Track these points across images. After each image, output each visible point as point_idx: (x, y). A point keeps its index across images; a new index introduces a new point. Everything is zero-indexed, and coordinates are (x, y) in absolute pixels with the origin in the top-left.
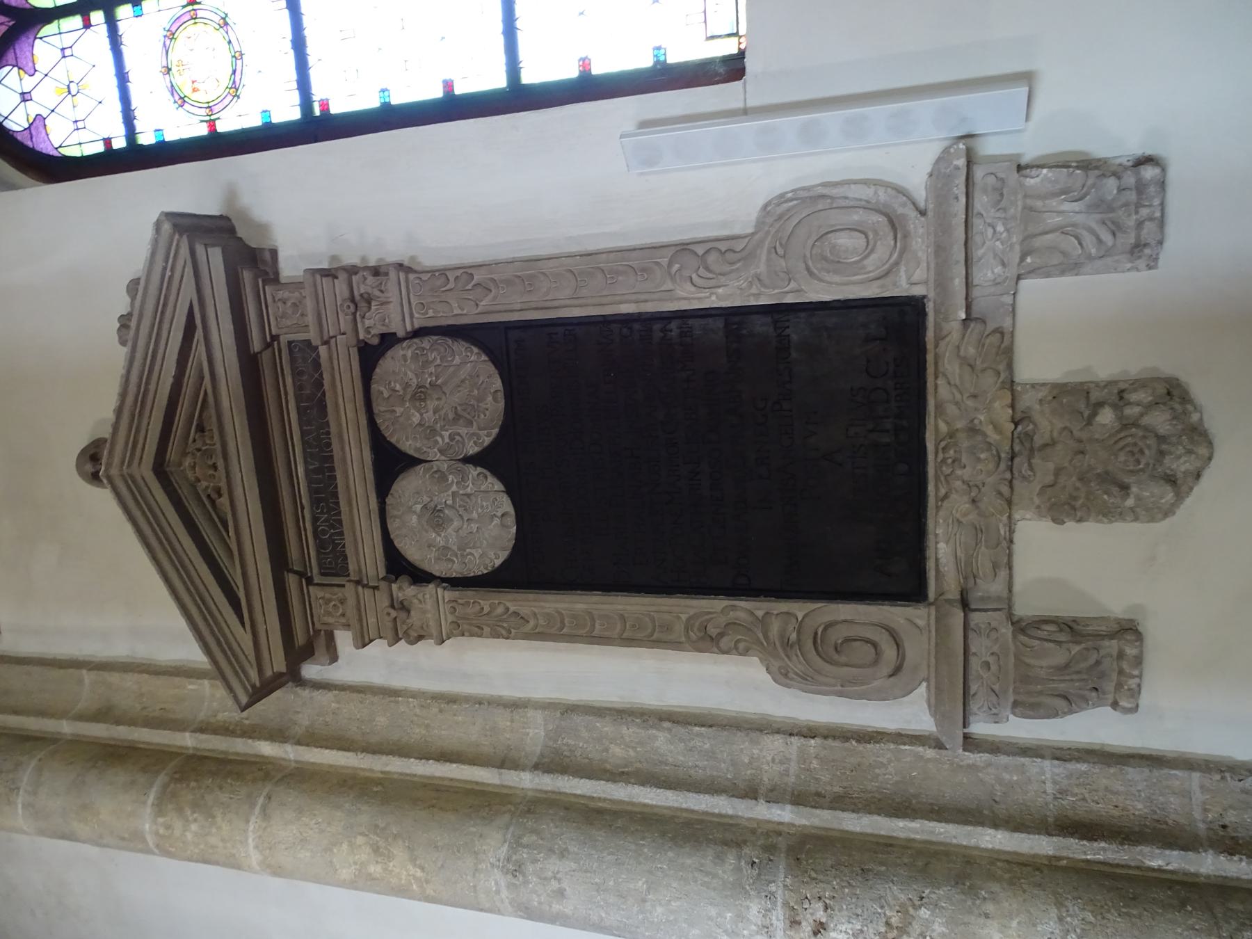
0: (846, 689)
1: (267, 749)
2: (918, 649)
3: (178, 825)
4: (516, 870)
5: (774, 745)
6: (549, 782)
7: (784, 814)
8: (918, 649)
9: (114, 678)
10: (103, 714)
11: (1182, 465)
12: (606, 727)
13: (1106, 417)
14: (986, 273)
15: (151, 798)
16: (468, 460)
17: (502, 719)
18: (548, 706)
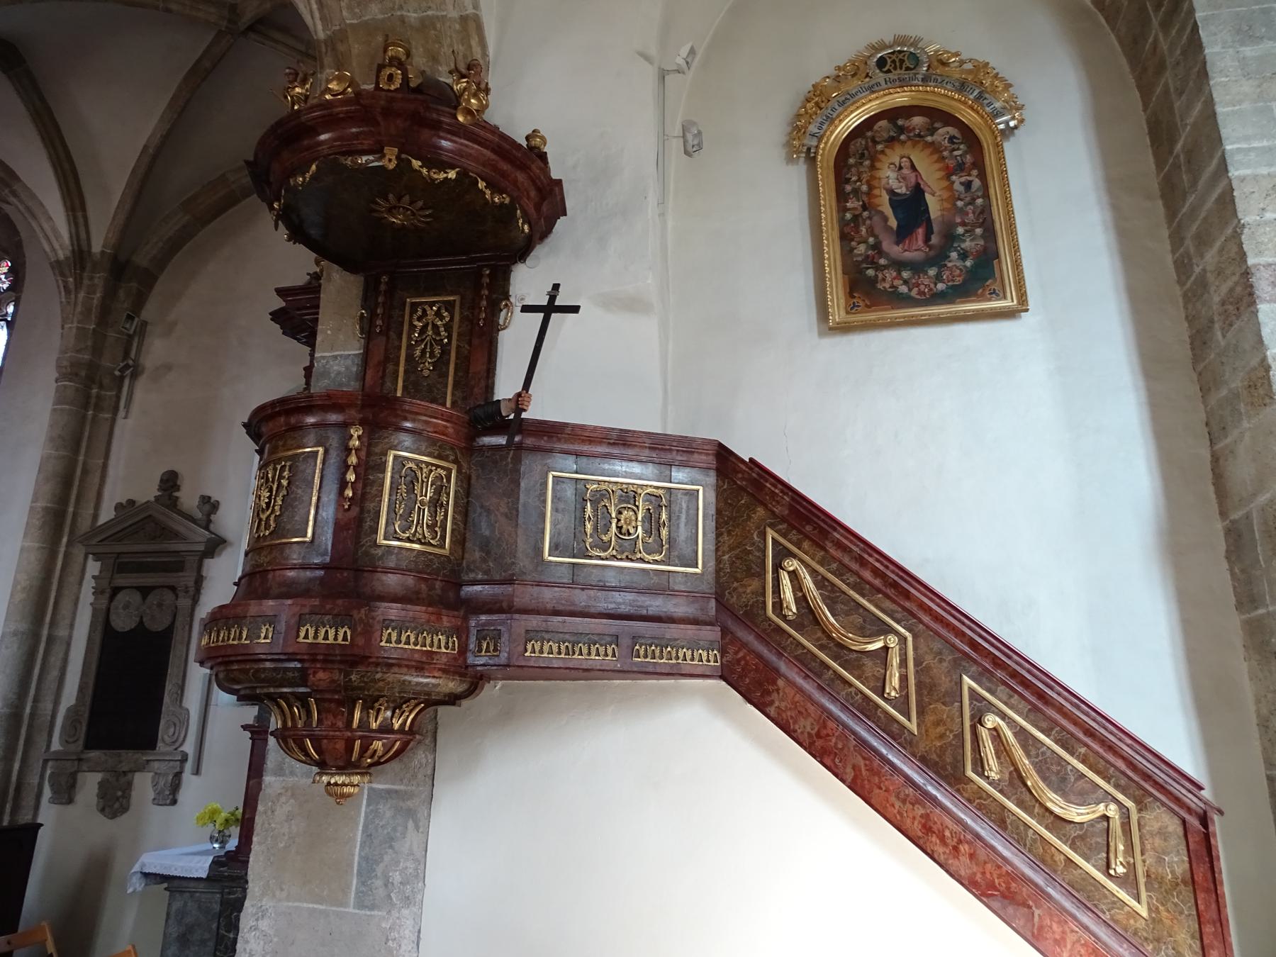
0: (63, 727)
1: (65, 540)
2: (72, 748)
3: (38, 516)
4: (15, 634)
5: (50, 706)
6: (44, 639)
7: (28, 710)
8: (72, 748)
9: (98, 474)
10: (85, 471)
11: (107, 810)
12: (61, 655)
13: (120, 793)
14: (156, 765)
15: (49, 505)
16: (142, 617)
17: (67, 621)
18: (70, 637)
